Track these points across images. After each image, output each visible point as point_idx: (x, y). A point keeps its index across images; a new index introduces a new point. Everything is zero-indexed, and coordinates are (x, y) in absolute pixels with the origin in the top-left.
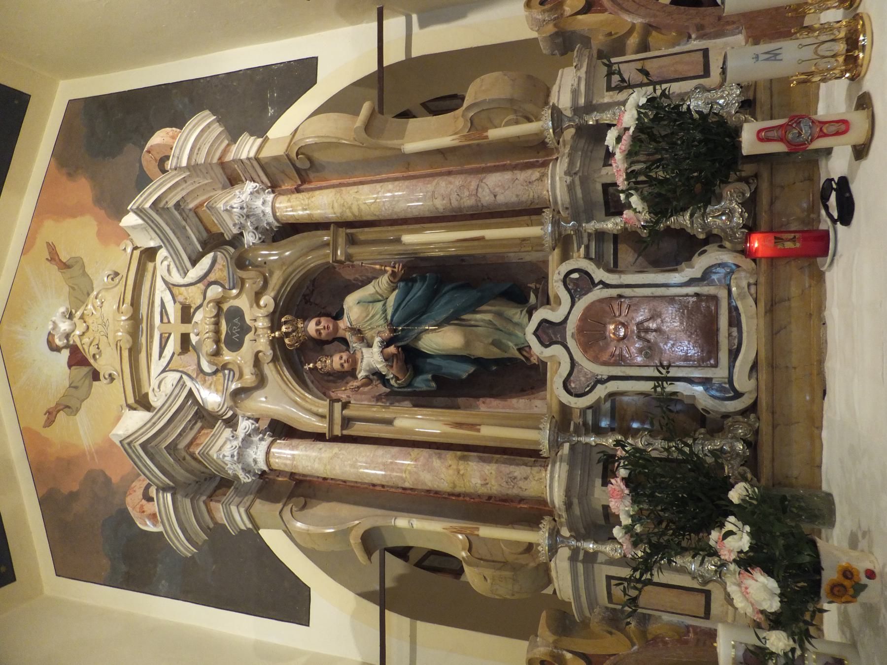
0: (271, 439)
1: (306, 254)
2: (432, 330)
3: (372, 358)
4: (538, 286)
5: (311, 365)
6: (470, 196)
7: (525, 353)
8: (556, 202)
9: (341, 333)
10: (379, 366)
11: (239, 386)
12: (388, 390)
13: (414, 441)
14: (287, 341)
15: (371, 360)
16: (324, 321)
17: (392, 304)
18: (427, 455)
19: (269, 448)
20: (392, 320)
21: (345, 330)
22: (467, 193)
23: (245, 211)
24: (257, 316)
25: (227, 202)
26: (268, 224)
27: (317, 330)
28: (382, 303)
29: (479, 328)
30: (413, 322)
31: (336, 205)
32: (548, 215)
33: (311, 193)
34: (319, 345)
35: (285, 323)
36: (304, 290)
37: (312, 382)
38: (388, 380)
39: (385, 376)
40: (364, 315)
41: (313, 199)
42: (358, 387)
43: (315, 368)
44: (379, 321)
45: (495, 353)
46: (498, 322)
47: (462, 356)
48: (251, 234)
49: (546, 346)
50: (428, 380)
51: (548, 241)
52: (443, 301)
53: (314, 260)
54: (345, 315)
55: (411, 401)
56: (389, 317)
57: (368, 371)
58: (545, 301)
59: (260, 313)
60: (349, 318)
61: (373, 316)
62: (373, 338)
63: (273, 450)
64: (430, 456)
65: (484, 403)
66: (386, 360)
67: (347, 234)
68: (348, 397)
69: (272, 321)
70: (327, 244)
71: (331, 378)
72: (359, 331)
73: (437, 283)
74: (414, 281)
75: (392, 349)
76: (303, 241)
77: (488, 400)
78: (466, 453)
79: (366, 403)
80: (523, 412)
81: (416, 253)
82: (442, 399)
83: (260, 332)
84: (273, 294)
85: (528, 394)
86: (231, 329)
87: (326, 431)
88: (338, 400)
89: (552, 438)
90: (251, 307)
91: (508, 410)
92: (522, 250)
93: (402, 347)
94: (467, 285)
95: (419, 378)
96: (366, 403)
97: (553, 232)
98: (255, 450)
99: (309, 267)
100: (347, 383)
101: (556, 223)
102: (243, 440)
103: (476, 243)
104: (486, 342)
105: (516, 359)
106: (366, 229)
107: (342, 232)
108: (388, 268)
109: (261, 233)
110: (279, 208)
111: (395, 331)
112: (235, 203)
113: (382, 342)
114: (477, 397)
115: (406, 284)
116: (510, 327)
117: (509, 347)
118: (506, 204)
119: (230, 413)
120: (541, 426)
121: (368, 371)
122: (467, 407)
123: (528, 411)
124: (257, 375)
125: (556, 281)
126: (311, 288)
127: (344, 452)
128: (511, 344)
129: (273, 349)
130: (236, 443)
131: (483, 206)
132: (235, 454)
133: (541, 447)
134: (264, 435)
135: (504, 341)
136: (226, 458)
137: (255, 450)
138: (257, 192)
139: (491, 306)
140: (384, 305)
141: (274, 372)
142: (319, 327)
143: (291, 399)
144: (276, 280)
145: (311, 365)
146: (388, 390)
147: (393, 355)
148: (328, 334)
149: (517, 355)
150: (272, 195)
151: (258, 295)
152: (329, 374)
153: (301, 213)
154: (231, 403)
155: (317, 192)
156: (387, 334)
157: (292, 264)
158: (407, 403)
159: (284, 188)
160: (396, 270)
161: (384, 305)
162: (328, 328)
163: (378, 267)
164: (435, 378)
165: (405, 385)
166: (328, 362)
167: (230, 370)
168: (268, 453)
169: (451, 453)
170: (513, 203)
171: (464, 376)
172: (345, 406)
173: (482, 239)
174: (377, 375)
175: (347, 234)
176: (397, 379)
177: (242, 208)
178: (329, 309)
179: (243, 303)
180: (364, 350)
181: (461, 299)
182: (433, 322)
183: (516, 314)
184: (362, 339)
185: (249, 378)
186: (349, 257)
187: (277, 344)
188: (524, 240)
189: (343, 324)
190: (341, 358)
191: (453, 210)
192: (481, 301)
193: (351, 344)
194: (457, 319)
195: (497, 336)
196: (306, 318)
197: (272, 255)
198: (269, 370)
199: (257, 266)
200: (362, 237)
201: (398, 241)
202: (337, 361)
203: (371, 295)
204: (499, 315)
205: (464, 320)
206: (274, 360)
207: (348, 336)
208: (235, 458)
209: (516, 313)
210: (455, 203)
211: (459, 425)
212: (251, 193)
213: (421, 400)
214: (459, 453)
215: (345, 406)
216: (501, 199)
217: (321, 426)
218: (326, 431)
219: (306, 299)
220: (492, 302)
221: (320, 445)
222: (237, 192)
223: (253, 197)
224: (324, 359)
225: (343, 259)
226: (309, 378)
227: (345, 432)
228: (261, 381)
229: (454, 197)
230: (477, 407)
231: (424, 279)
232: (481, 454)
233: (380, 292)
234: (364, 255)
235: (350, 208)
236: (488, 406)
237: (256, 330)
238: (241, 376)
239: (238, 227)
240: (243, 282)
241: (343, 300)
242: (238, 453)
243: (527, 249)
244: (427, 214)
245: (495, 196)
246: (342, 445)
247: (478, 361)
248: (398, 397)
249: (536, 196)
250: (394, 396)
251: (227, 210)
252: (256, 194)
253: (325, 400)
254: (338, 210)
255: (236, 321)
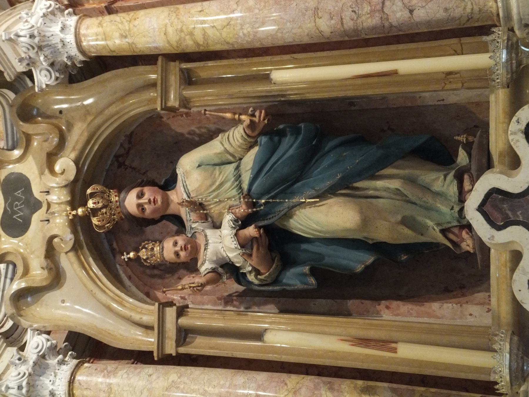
0: (75, 362)
1: (122, 99)
2: (310, 204)
3: (221, 243)
4: (471, 139)
5: (132, 255)
6: (372, 12)
7: (451, 236)
8: (508, 17)
9: (173, 209)
10: (231, 255)
11: (23, 285)
12: (241, 288)
13: (282, 363)
14: (95, 221)
15: (220, 246)
16: (149, 193)
17: (250, 165)
18: (311, 385)
19: (73, 375)
20: (249, 190)
21: (181, 204)
22: (367, 9)
23: (37, 40)
24: (51, 187)
25: (8, 28)
26: (70, 58)
27: (139, 206)
28: (234, 165)
29: (381, 200)
30: (283, 192)
31: (170, 30)
32: (500, 34)
33: (132, 14)
34: (139, 226)
35: (92, 195)
36: (116, 149)
37: (130, 278)
38: (244, 274)
39: (238, 268)
40: (208, 182)
41: (136, 22)
42: (203, 285)
43: (138, 259)
44: (230, 191)
45: (407, 236)
46: (409, 192)
47: (354, 240)
48: (44, 72)
49: (499, 228)
50: (305, 275)
51: (502, 74)
52: (326, 162)
53: (137, 106)
54: (179, 184)
55: (276, 304)
56: (245, 186)
57: (215, 262)
58: (484, 161)
59: (54, 182)
60: (185, 187)
61: (222, 184)
62: (221, 215)
63: (79, 378)
64: (316, 387)
65: (387, 307)
66: (242, 246)
67: (181, 70)
68: (183, 298)
69: (72, 193)
70: (153, 85)
71: (156, 272)
72: (201, 206)
73: (316, 137)
74: (282, 134)
75: (251, 231)
76: (115, 81)
77: (395, 304)
78: (371, 383)
79: (209, 307)
80: (452, 322)
81: (283, 96)
82: (323, 301)
83: (54, 208)
84: (73, 155)
85: (455, 297)
86: (11, 206)
87: (154, 348)
88: (171, 304)
89: (515, 365)
90: (42, 173)
91: (426, 320)
92: (448, 87)
93: (265, 227)
94: (360, 139)
95: (288, 271)
96: (209, 307)
97: (509, 60)
98: (52, 378)
99: (126, 117)
100: (180, 279)
101: (513, 47)
102: (35, 364)
103: (376, 80)
104: (393, 220)
105: (437, 245)
106: (210, 64)
107: (175, 67)
108: (243, 117)
109: (58, 71)
110: (85, 36)
111: (254, 205)
112: (22, 29)
113: (235, 221)
114: (377, 299)
115: (271, 139)
116: (429, 200)
117: (427, 227)
118: (428, 23)
119: (9, 324)
120: (496, 347)
121: (215, 262)
122: (361, 314)
123: (459, 322)
124: (50, 270)
125: (514, 133)
126: (126, 146)
127: (185, 379)
128: (430, 223)
129: (74, 232)
130: (24, 369)
131: (391, 26)
132: (24, 384)
133: (493, 378)
134: (65, 356)
135: (420, 218)
136: (11, 391)
137: (52, 378)
138: (53, 13)
139: (397, 168)
140: (238, 168)
141: (76, 265)
142: (141, 201)
143: (101, 303)
144: (77, 135)
145: (132, 255)
146: (241, 288)
147: (253, 239)
148: (154, 211)
149: (441, 239)
150: (75, 18)
151: (51, 158)
152: (154, 267)
153: (118, 42)
154: (11, 311)
155: (142, 13)
156: (242, 210)
157: (101, 112)
158: (271, 308)
159: (87, 6)
160: (256, 119)
161: (238, 168)
162: (155, 201)
163: (228, 115)
164: (314, 272)
165: (269, 281)
166: (157, 249)
167: (8, 263)
168: (71, 382)
169: (348, 382)
170: (439, 22)
171: (359, 268)
172: (182, 311)
173: (394, 73)
174: (228, 268)
175: (181, 70)
176: (258, 272)
177: (32, 36)
178: (152, 175)
179: (30, 169)
180: (209, 232)
181: (353, 158)
182: (312, 192)
183: (443, 183)
184: (205, 218)
185: (38, 274)
186: (185, 102)
187: (80, 225)
188: (449, 74)
189: (177, 196)
190: (175, 244)
191: (346, 33)
192: (385, 161)
193: (187, 224)
194: (348, 188)
195: (409, 211)
196: (122, 188)
197: (61, 103)
198: (68, 262)
199: (49, 117)
200: (204, 74)
201: (266, 78)
202: (169, 249)
203: (217, 154)
204: (411, 181)
205: (357, 189)
206: (76, 248)
207: (184, 212)
208: (24, 391)
209: (438, 178)
210: (349, 24)
211: (364, 342)
212: (44, 15)
213: (293, 303)
214: (360, 383)
215: (182, 311)
216: (420, 15)
217: (147, 341)
218: (154, 348)
219: (119, 161)
220: (399, 162)
221: (150, 369)
222: (23, 14)
223: (47, 21)
224: (150, 246)
225: (177, 104)
226: (125, 272)
227: (182, 350)
228: (56, 278)
229: (348, 14)
230: (378, 313)
231: (297, 132)
232: (395, 386)
233: (231, 150)
234: (206, 99)
235: (191, 34)
236: (394, 315)
237: (49, 205)
238: (26, 271)
239: (25, 63)
240: (28, 139)
241: (174, 162)
242: (28, 383)
243: (454, 86)
244: (306, 40)
245: (411, 11)
246: (182, 369)
247: (378, 247)
248: (257, 299)
249: (476, 8)
250: (251, 296)
251: (10, 40)
252: (50, 17)
253: (153, 305)
254: (173, 37)
255: (18, 193)
